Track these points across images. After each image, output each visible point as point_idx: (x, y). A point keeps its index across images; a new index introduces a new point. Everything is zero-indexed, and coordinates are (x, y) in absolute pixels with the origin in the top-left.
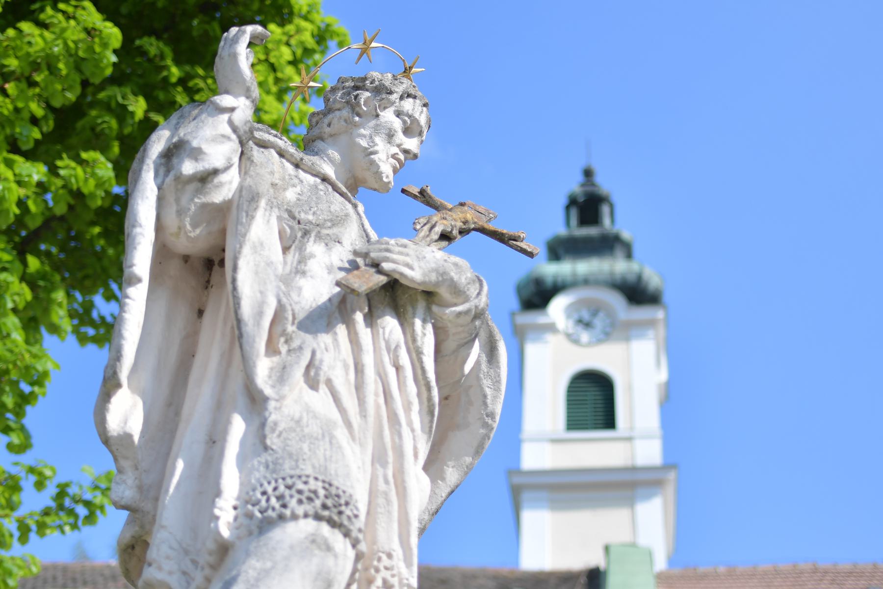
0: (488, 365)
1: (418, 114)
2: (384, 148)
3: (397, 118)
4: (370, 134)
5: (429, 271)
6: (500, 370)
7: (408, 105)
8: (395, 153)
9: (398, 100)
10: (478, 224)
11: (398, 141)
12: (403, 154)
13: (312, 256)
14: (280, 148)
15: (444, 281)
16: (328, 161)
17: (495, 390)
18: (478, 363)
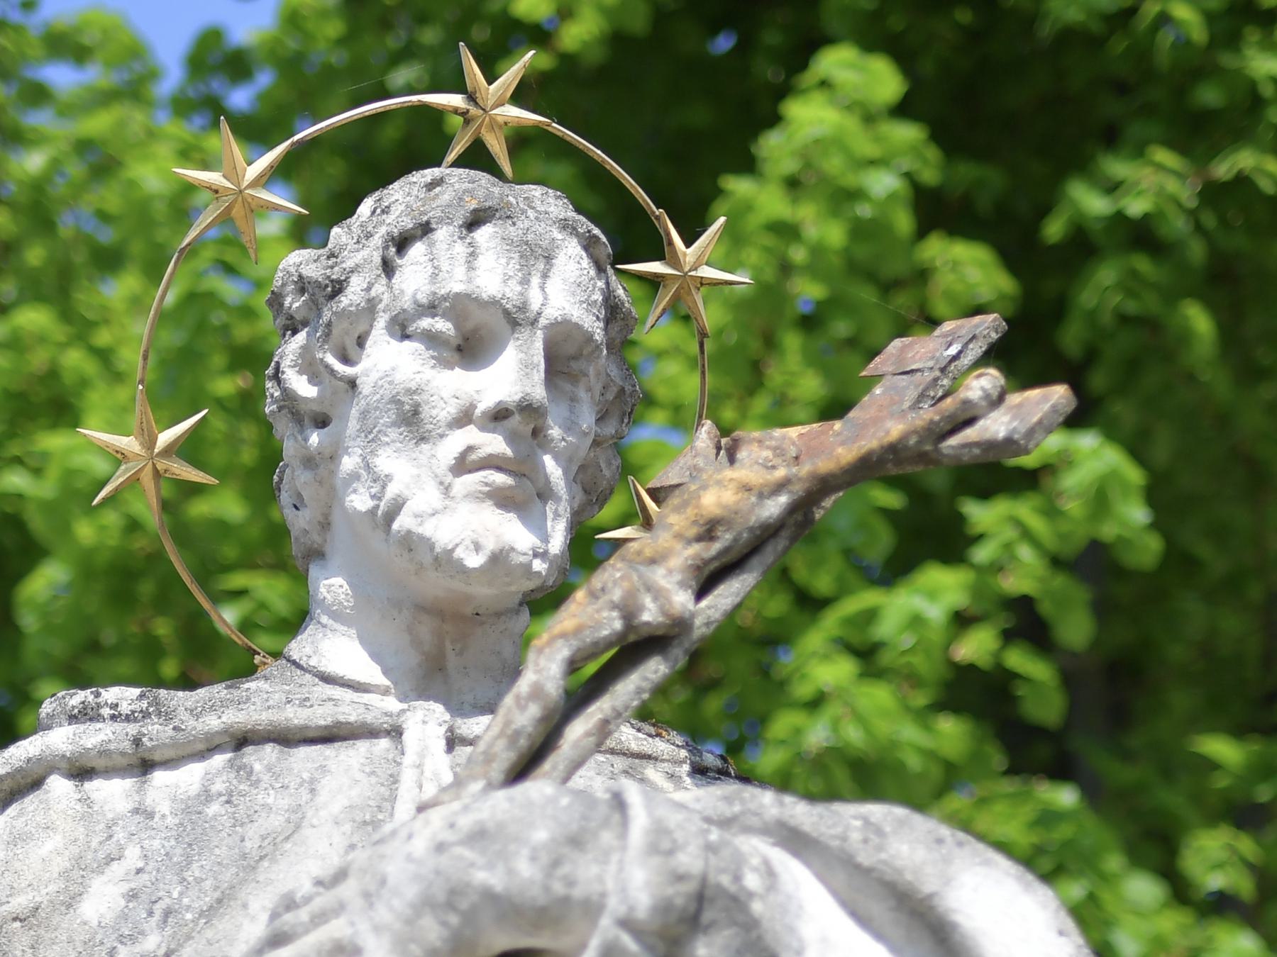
1: (460, 271)
2: (415, 471)
3: (407, 343)
5: (409, 922)
9: (379, 288)
10: (800, 479)
12: (493, 431)
15: (469, 917)
16: (331, 622)
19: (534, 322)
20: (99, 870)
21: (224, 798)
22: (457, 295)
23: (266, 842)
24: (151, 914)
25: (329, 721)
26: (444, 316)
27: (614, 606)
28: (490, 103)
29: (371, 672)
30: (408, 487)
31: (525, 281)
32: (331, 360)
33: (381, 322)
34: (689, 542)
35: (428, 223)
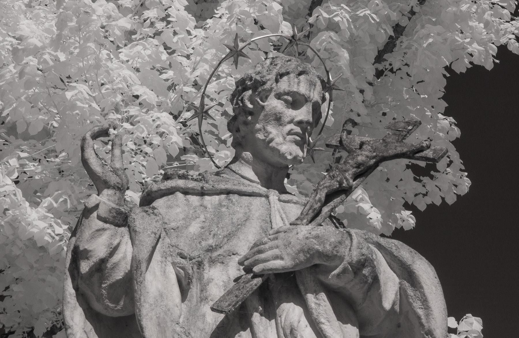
0: (413, 288)
1: (296, 86)
2: (277, 132)
3: (279, 101)
4: (263, 126)
6: (423, 289)
7: (284, 85)
8: (289, 129)
9: (274, 85)
10: (379, 156)
11: (287, 120)
13: (210, 280)
14: (182, 188)
16: (245, 163)
17: (425, 309)
18: (402, 291)
19: (311, 101)
20: (194, 220)
21: (227, 207)
22: (294, 92)
23: (239, 220)
24: (210, 234)
25: (251, 191)
26: (291, 96)
27: (337, 181)
28: (297, 39)
29: (255, 178)
30: (275, 136)
31: (310, 91)
32: (259, 100)
33: (273, 94)
34: (354, 168)
35: (289, 72)
